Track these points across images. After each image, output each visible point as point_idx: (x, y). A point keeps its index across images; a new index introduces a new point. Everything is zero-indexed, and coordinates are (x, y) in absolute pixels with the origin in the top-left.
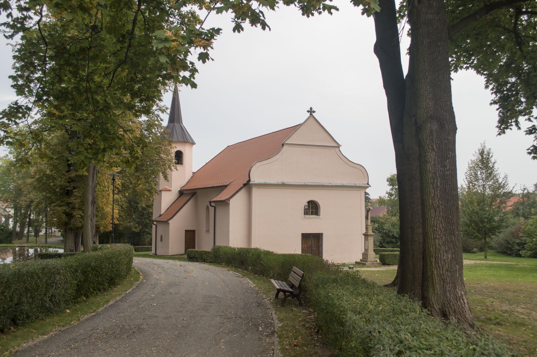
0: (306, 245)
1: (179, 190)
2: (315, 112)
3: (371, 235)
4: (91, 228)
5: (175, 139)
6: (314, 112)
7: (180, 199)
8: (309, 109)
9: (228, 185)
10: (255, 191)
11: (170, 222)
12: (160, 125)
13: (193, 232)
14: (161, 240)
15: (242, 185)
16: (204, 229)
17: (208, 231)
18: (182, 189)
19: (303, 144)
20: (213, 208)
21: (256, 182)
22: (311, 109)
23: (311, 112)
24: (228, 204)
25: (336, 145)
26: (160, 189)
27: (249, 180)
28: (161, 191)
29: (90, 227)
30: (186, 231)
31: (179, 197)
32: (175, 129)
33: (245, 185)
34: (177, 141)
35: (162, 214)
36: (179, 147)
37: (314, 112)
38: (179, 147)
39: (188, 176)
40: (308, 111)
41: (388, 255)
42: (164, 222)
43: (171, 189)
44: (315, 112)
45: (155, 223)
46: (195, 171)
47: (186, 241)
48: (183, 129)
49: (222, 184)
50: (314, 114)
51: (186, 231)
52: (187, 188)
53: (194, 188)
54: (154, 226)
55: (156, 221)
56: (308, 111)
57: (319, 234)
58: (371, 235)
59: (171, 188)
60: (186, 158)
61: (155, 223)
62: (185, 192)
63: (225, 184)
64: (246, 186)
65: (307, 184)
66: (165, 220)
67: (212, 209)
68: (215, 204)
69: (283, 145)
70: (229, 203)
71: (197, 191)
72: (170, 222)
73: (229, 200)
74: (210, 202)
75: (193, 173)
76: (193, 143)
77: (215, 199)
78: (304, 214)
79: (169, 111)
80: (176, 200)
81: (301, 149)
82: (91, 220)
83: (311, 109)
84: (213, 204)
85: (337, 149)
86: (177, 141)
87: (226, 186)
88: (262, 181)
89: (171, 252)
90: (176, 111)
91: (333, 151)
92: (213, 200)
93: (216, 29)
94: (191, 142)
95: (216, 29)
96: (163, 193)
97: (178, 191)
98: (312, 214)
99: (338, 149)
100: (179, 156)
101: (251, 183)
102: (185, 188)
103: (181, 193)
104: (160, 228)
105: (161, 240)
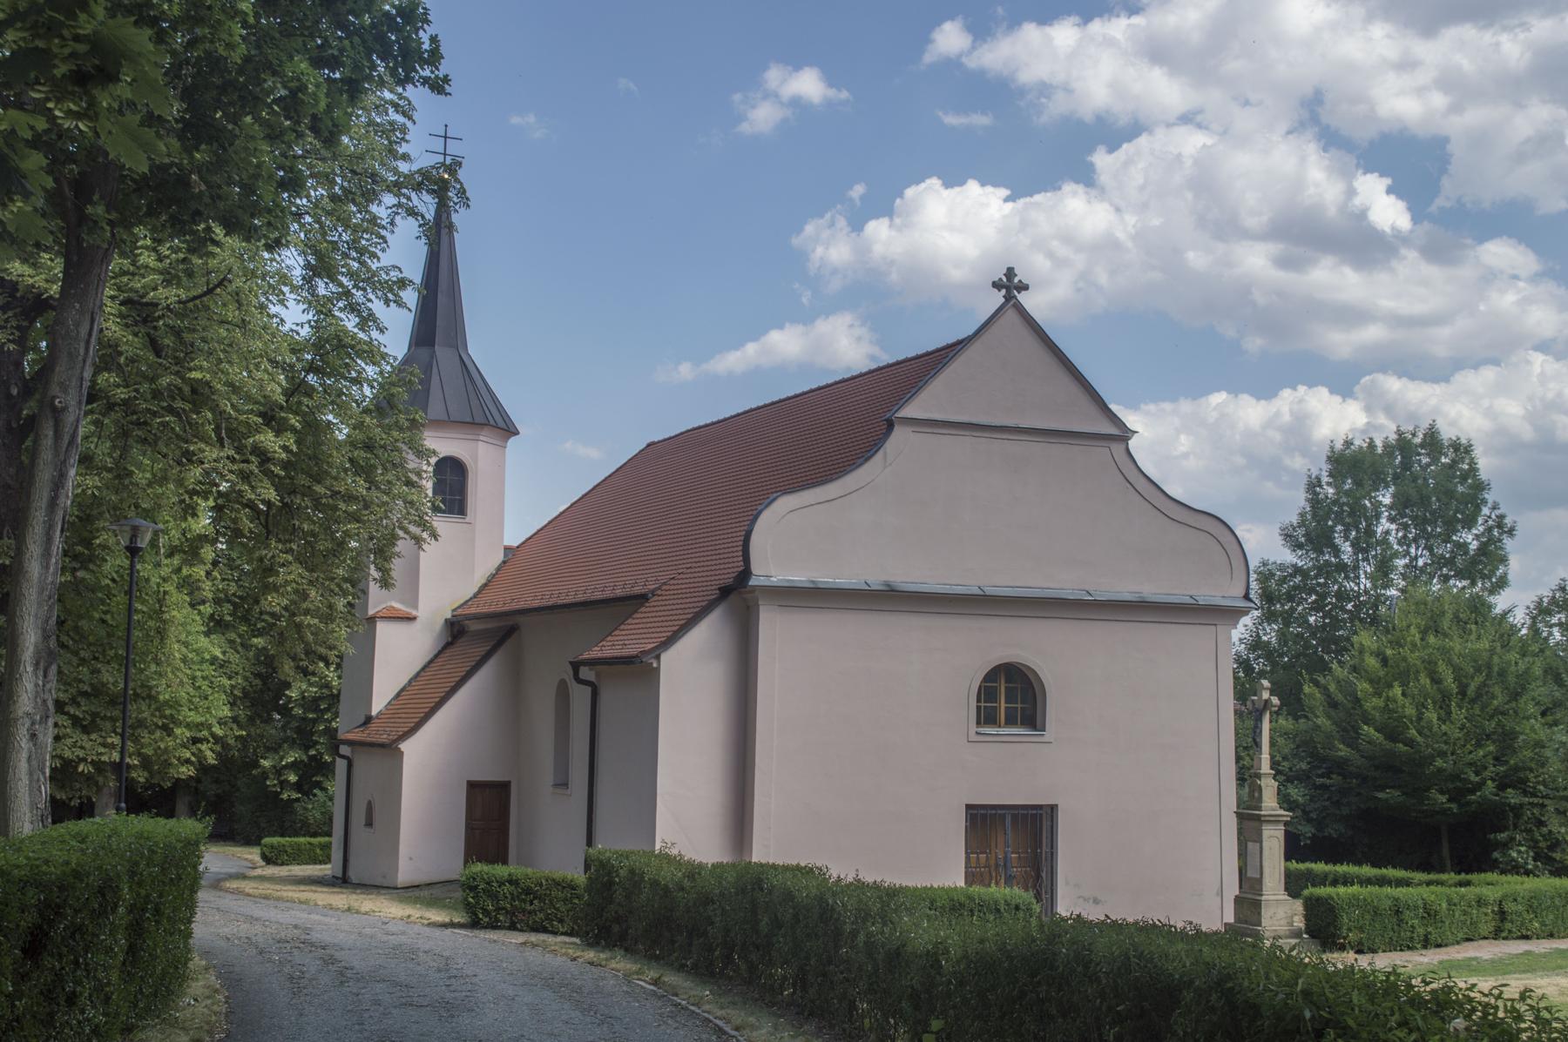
0: (983, 856)
1: (449, 616)
2: (1026, 288)
3: (1274, 820)
4: (31, 774)
5: (436, 409)
6: (1023, 287)
7: (448, 653)
8: (1000, 275)
9: (653, 592)
10: (772, 625)
11: (403, 746)
12: (372, 354)
13: (502, 788)
14: (369, 824)
15: (716, 594)
16: (547, 776)
17: (562, 784)
18: (460, 611)
19: (974, 421)
20: (589, 689)
21: (774, 580)
22: (1010, 273)
23: (1008, 289)
24: (653, 675)
25: (1114, 431)
26: (371, 612)
27: (746, 573)
28: (372, 620)
29: (23, 766)
30: (473, 786)
31: (447, 646)
32: (435, 369)
33: (725, 592)
34: (469, 419)
35: (374, 713)
36: (442, 444)
37: (1023, 287)
38: (442, 444)
39: (487, 563)
40: (997, 285)
41: (1354, 901)
42: (382, 746)
43: (414, 613)
44: (1026, 288)
45: (344, 750)
46: (515, 544)
47: (470, 828)
48: (468, 371)
49: (628, 591)
50: (1023, 298)
51: (473, 786)
52: (485, 610)
53: (506, 608)
54: (341, 765)
55: (350, 743)
56: (997, 285)
57: (1040, 807)
58: (1274, 820)
59: (416, 607)
60: (478, 491)
61: (344, 750)
62: (474, 626)
63: (637, 590)
64: (733, 597)
65: (989, 591)
66: (384, 738)
67: (580, 698)
68: (598, 675)
69: (890, 425)
70: (658, 669)
71: (521, 619)
72: (404, 746)
73: (658, 657)
74: (576, 666)
75: (507, 549)
76: (507, 430)
77: (595, 653)
78: (978, 723)
79: (410, 297)
80: (436, 656)
81: (966, 441)
82: (33, 736)
83: (1010, 273)
84: (585, 673)
85: (1117, 448)
86: (446, 419)
87: (642, 598)
88: (798, 576)
89: (406, 873)
90: (442, 299)
91: (1099, 452)
92: (586, 656)
93: (1387, 181)
94: (501, 424)
95: (1387, 181)
96: (382, 628)
97: (442, 621)
98: (1011, 721)
99: (1121, 447)
100: (452, 477)
101: (753, 582)
102: (473, 610)
103: (456, 630)
104: (367, 768)
105: (369, 824)
